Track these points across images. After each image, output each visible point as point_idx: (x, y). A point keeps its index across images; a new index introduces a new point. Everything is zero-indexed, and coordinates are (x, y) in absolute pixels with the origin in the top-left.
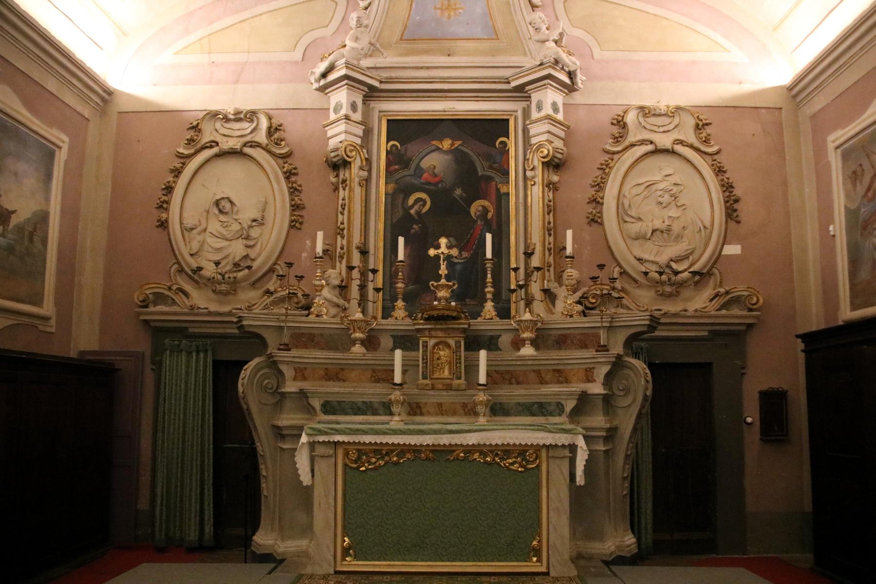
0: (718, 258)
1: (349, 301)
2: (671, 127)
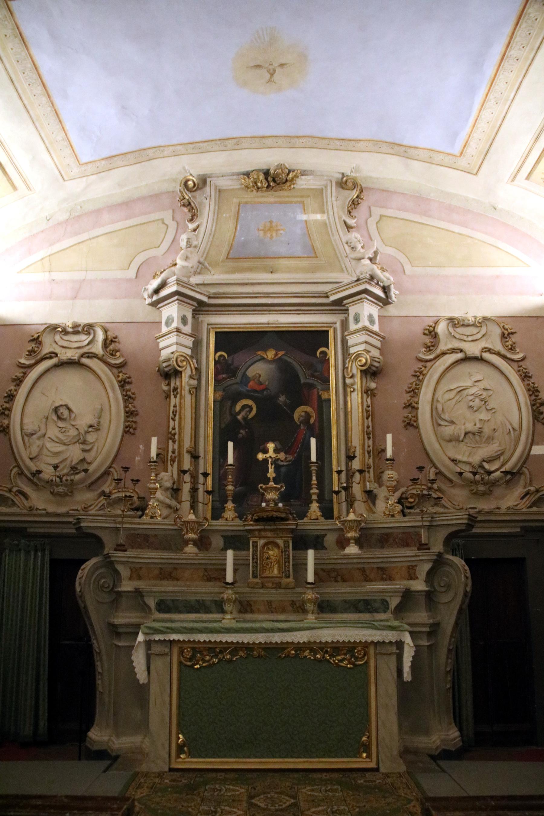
0: (527, 457)
1: (180, 502)
2: (479, 336)
